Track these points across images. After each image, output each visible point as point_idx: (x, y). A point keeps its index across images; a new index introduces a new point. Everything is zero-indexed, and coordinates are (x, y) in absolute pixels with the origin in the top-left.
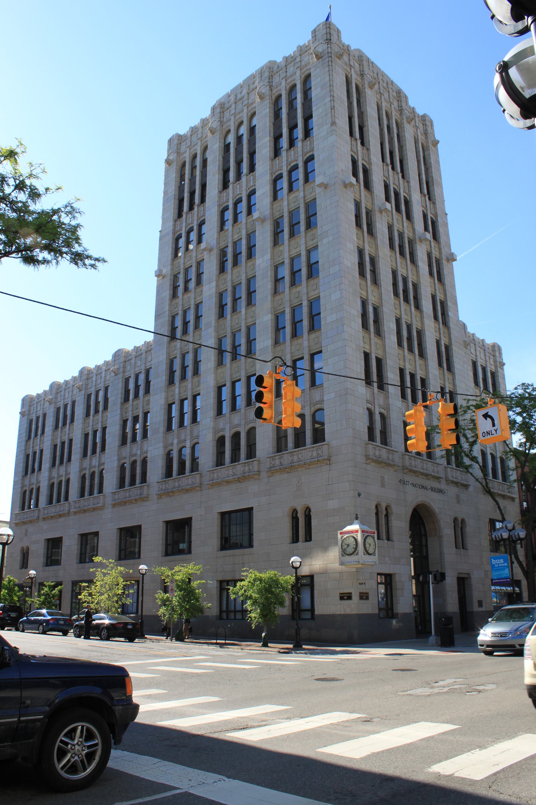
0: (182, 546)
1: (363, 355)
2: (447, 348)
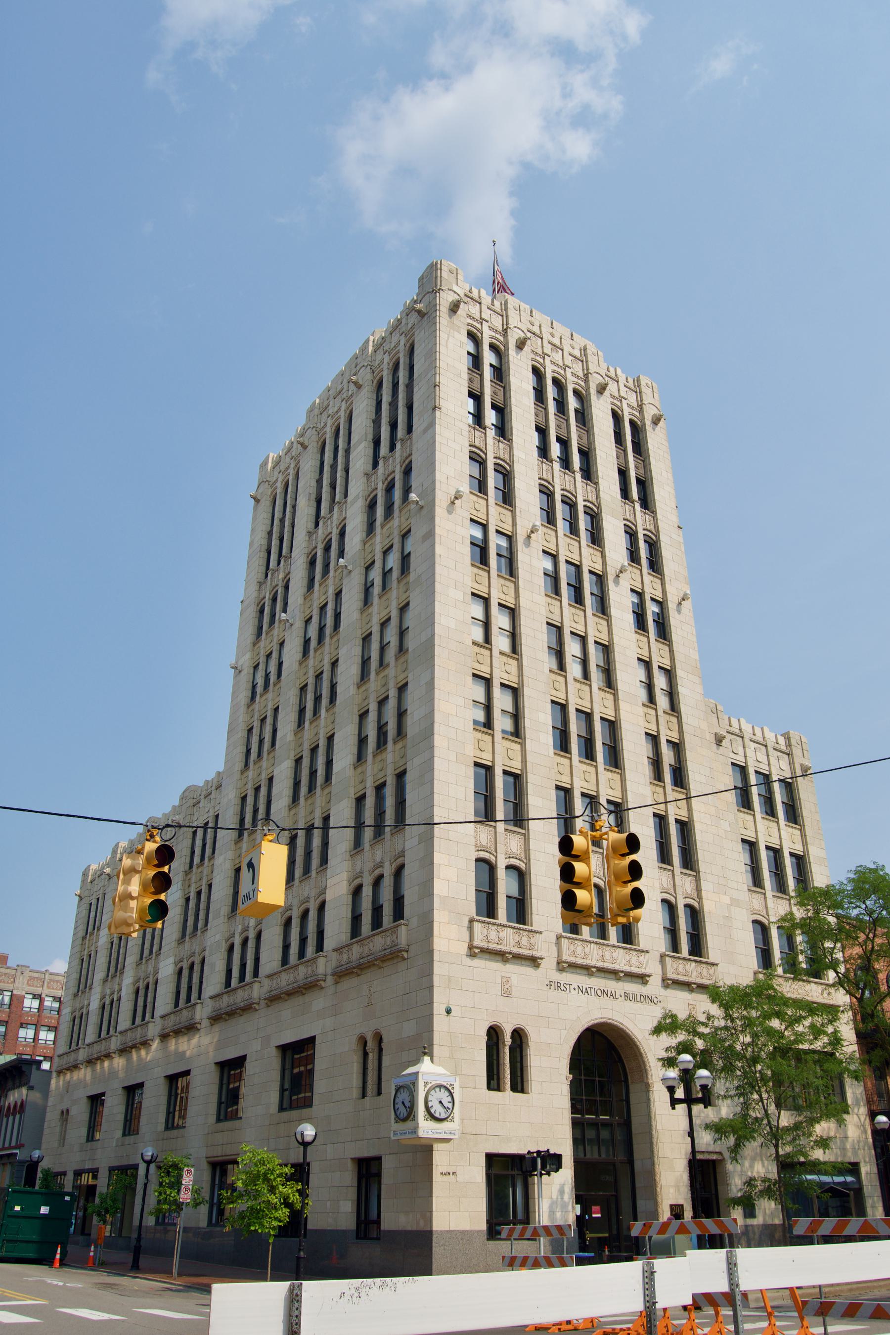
2: (677, 747)
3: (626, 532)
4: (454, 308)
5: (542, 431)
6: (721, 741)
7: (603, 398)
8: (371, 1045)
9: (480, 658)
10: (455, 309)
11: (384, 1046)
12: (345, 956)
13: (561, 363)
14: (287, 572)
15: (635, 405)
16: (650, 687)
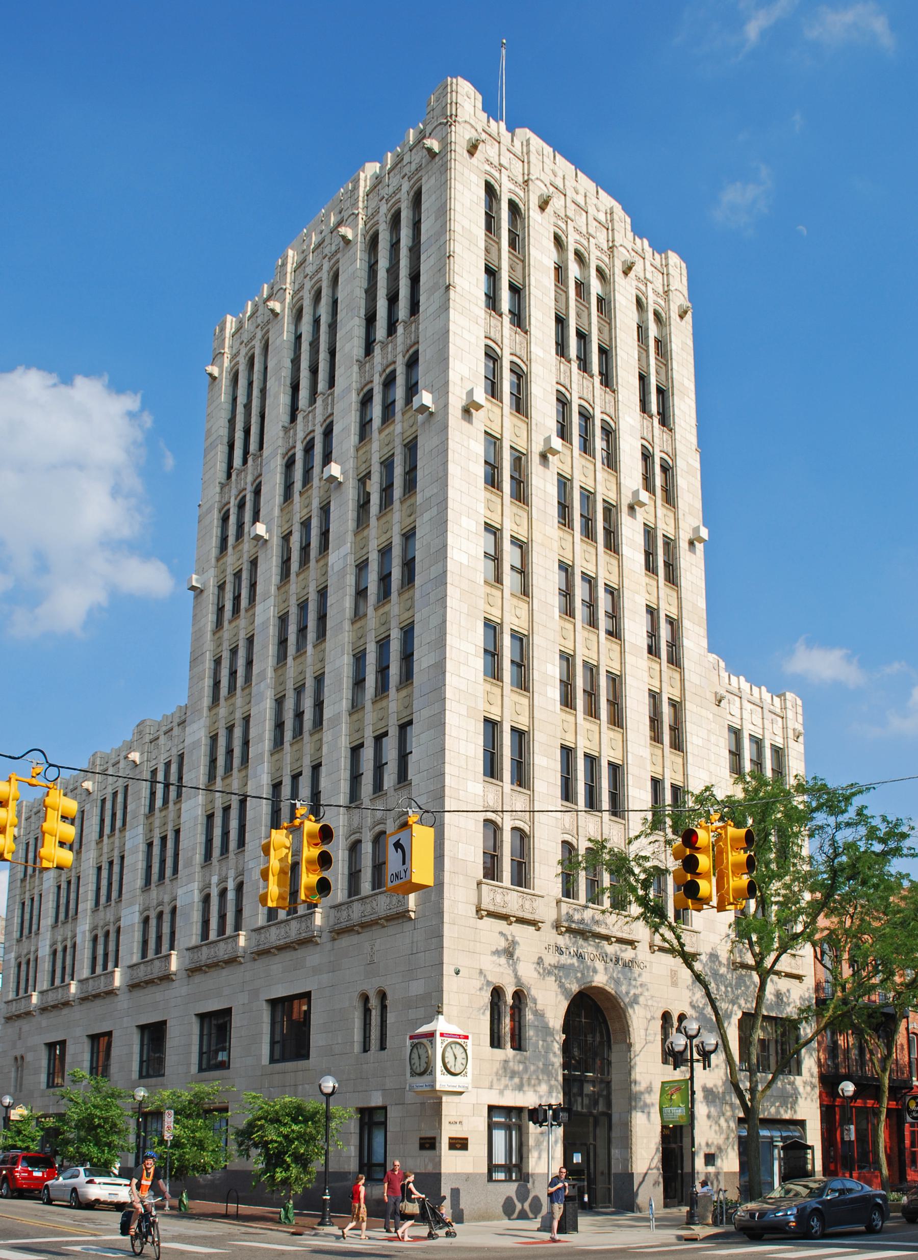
0: (222, 1057)
1: (481, 726)
2: (677, 706)
3: (558, 399)
4: (472, 149)
5: (492, 273)
6: (720, 701)
7: (474, 160)
8: (374, 1002)
9: (491, 599)
10: (473, 150)
11: (388, 1002)
12: (345, 914)
13: (584, 231)
14: (256, 474)
15: (661, 291)
16: (496, 558)
